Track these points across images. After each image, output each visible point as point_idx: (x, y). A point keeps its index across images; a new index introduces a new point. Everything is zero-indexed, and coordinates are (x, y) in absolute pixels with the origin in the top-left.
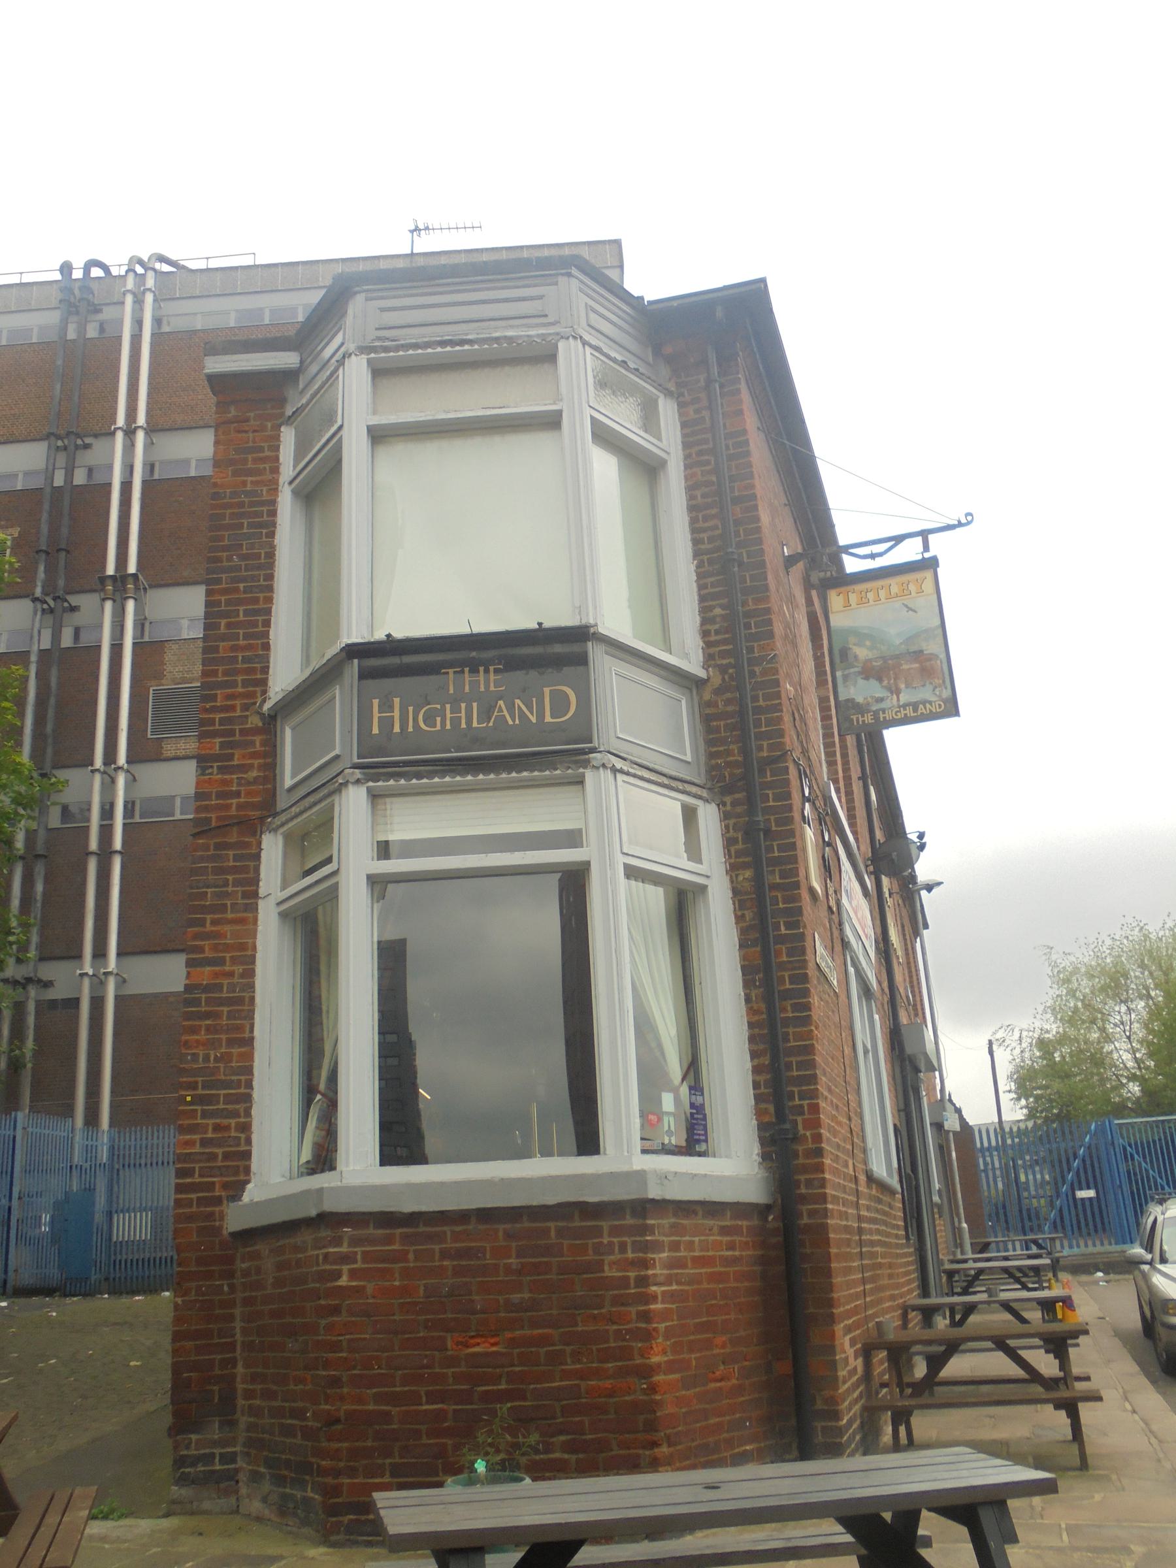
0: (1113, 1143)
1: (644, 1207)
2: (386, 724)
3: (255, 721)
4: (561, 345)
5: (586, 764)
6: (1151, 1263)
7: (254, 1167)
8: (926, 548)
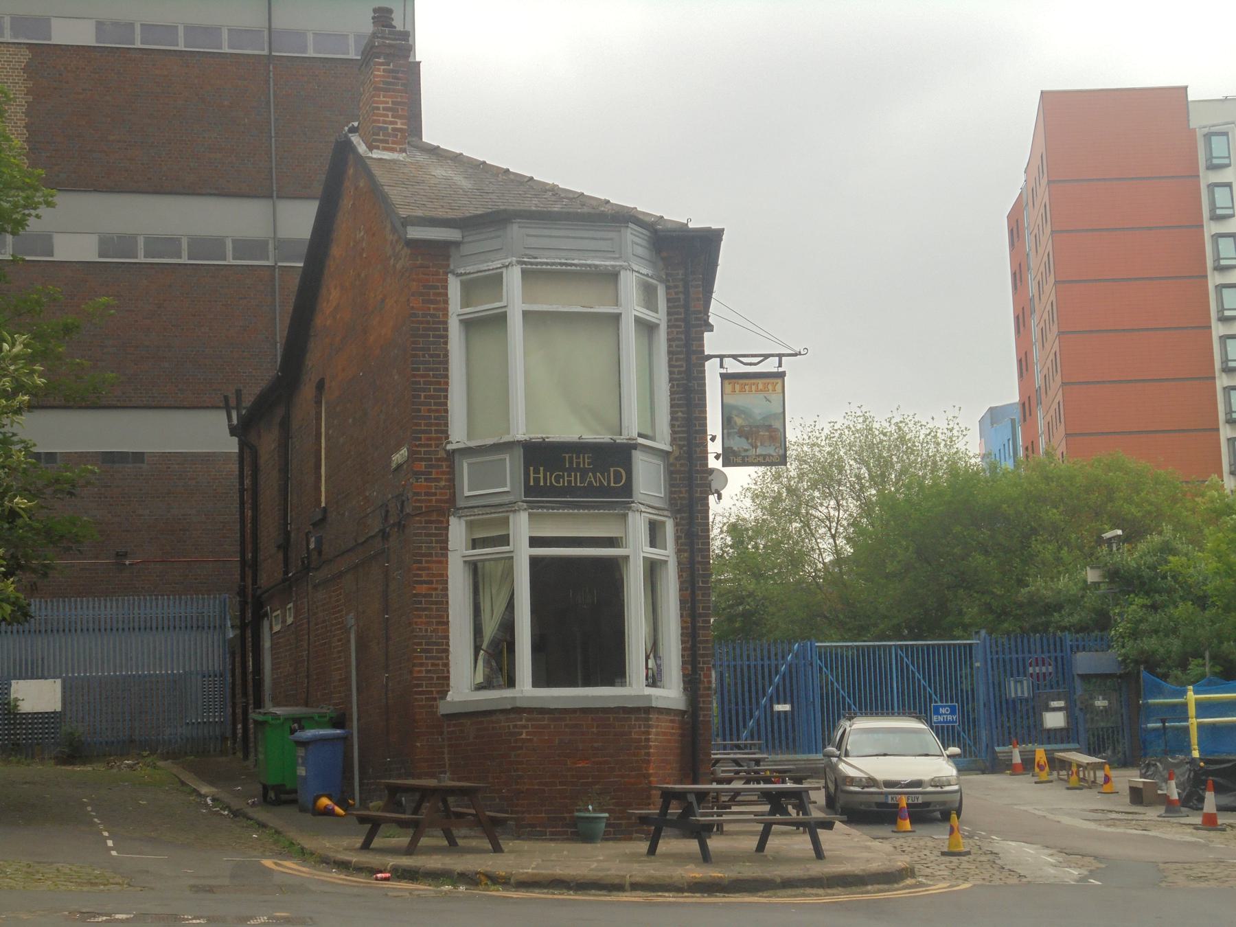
0: (811, 664)
1: (648, 710)
2: (537, 480)
3: (442, 454)
4: (622, 273)
5: (630, 508)
6: (839, 757)
7: (452, 684)
8: (780, 365)
